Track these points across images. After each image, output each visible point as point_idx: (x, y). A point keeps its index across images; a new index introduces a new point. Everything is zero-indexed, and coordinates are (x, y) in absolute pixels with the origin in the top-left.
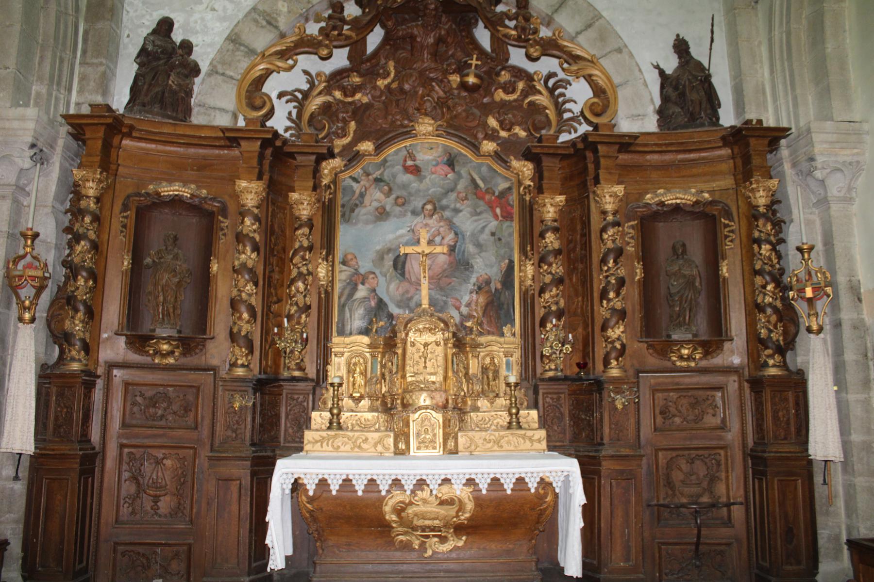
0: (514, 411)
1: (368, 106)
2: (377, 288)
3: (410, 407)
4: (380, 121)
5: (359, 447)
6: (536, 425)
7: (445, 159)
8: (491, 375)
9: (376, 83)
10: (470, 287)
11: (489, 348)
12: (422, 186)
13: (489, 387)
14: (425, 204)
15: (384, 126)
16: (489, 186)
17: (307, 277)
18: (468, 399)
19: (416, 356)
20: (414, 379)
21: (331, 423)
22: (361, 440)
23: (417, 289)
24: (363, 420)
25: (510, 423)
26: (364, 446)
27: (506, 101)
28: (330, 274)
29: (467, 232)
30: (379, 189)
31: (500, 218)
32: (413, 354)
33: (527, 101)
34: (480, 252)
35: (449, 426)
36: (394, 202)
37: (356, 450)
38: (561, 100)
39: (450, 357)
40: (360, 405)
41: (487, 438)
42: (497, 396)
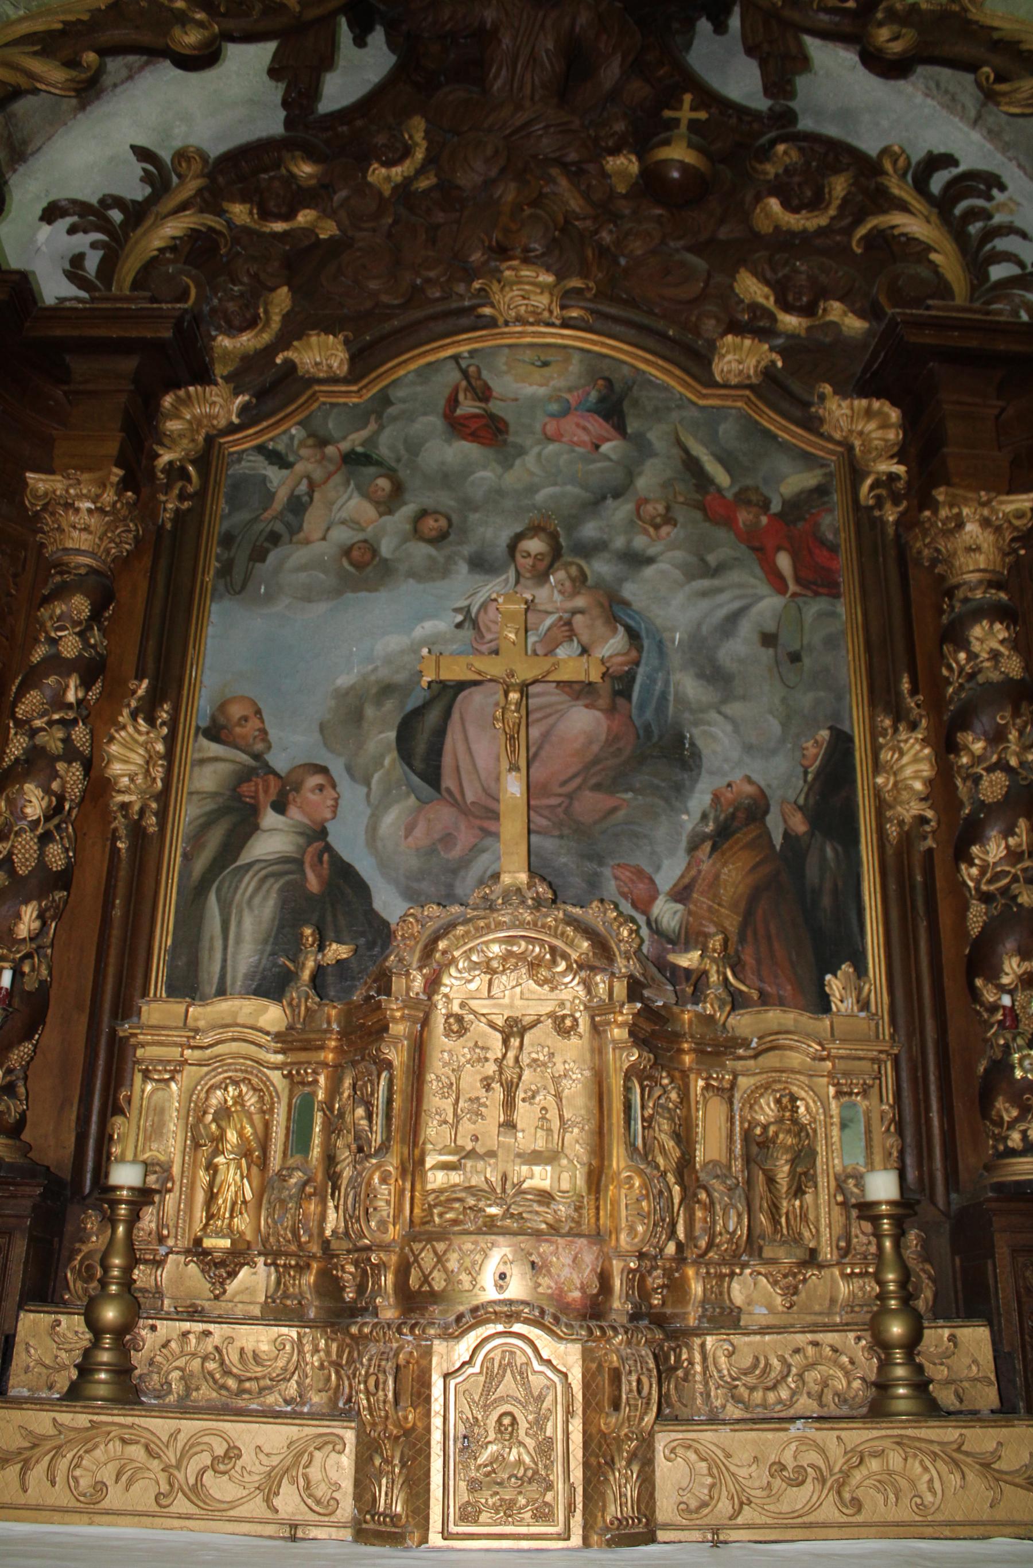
0: (896, 1329)
1: (335, 246)
2: (329, 826)
3: (435, 1310)
4: (373, 285)
5: (196, 1491)
6: (989, 1397)
7: (594, 396)
8: (783, 1172)
9: (365, 177)
10: (689, 821)
11: (770, 1060)
12: (513, 478)
13: (775, 1222)
14: (519, 537)
15: (385, 299)
16: (749, 482)
17: (61, 766)
18: (691, 1272)
19: (470, 1081)
20: (455, 1177)
21: (86, 1369)
22: (206, 1459)
23: (487, 833)
24: (232, 1357)
25: (883, 1386)
26: (220, 1488)
27: (792, 234)
28: (158, 772)
29: (673, 630)
30: (358, 488)
31: (792, 587)
32: (458, 1070)
33: (862, 231)
34: (724, 701)
35: (616, 1406)
36: (408, 527)
37: (181, 1505)
38: (975, 228)
39: (616, 1084)
40: (233, 1286)
41: (788, 1458)
42: (812, 1259)
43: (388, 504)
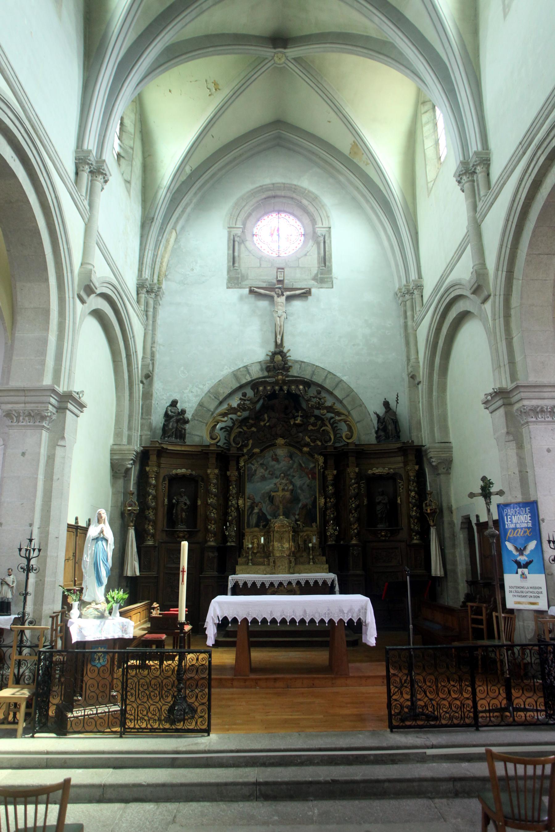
43: (266, 470)
